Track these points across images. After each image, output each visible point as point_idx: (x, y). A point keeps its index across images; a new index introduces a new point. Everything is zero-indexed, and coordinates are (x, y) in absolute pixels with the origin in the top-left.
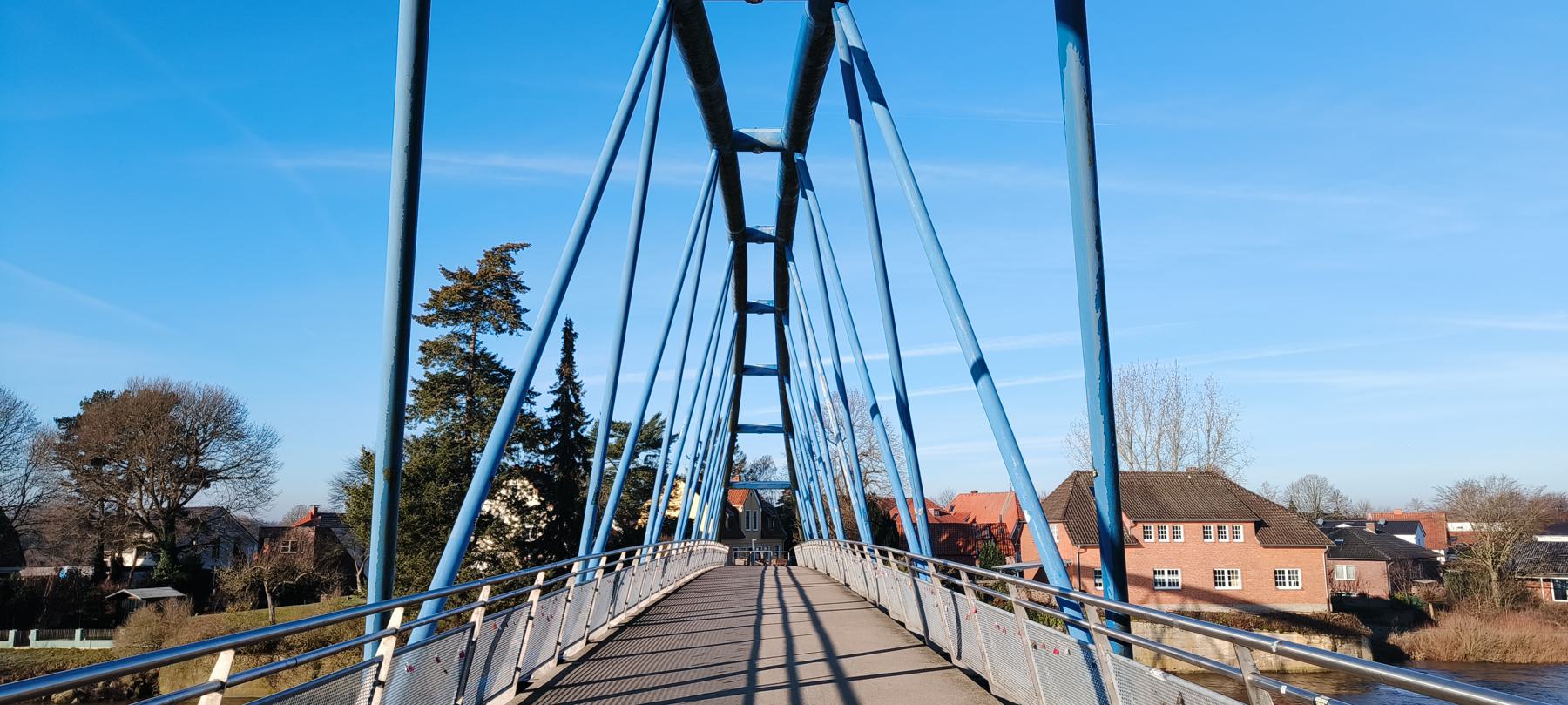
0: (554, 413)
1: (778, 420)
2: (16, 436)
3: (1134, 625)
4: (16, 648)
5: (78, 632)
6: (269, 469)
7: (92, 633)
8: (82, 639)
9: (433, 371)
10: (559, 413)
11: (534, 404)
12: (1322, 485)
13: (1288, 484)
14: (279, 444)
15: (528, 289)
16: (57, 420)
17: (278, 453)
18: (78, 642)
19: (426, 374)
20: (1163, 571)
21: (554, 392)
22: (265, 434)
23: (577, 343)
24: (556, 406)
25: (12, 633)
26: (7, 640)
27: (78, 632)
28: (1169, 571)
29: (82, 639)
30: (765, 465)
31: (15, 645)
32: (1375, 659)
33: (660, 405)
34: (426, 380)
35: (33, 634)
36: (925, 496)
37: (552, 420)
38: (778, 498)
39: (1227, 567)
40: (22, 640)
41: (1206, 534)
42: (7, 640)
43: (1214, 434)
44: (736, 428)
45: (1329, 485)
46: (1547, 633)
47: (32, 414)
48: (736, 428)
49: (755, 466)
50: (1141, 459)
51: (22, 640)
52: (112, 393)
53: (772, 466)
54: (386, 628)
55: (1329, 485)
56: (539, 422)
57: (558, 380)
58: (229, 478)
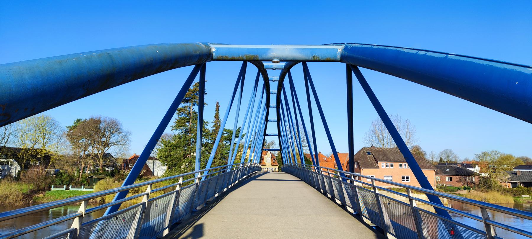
0: (213, 129)
1: (277, 133)
2: (55, 131)
3: (362, 178)
4: (66, 190)
5: (83, 186)
6: (128, 142)
7: (86, 187)
8: (84, 188)
9: (180, 116)
10: (215, 128)
11: (208, 125)
12: (450, 152)
13: (440, 152)
14: (132, 135)
15: (207, 94)
16: (67, 127)
17: (132, 138)
18: (83, 189)
19: (179, 117)
20: (387, 177)
21: (213, 122)
22: (128, 132)
23: (220, 109)
24: (214, 126)
25: (65, 186)
26: (63, 188)
27: (83, 186)
28: (389, 177)
29: (84, 188)
30: (273, 143)
31: (66, 189)
32: (437, 197)
33: (240, 125)
34: (178, 119)
35: (70, 187)
36: (338, 151)
37: (213, 131)
38: (276, 153)
39: (406, 175)
40: (67, 188)
41: (401, 166)
42: (63, 188)
43: (408, 136)
44: (265, 135)
45: (453, 152)
46: (503, 197)
47: (60, 125)
48: (265, 135)
49: (270, 144)
50: (386, 144)
51: (67, 188)
52: (81, 120)
53: (275, 144)
54: (125, 197)
55: (453, 152)
56: (209, 131)
57: (214, 119)
58: (117, 145)
